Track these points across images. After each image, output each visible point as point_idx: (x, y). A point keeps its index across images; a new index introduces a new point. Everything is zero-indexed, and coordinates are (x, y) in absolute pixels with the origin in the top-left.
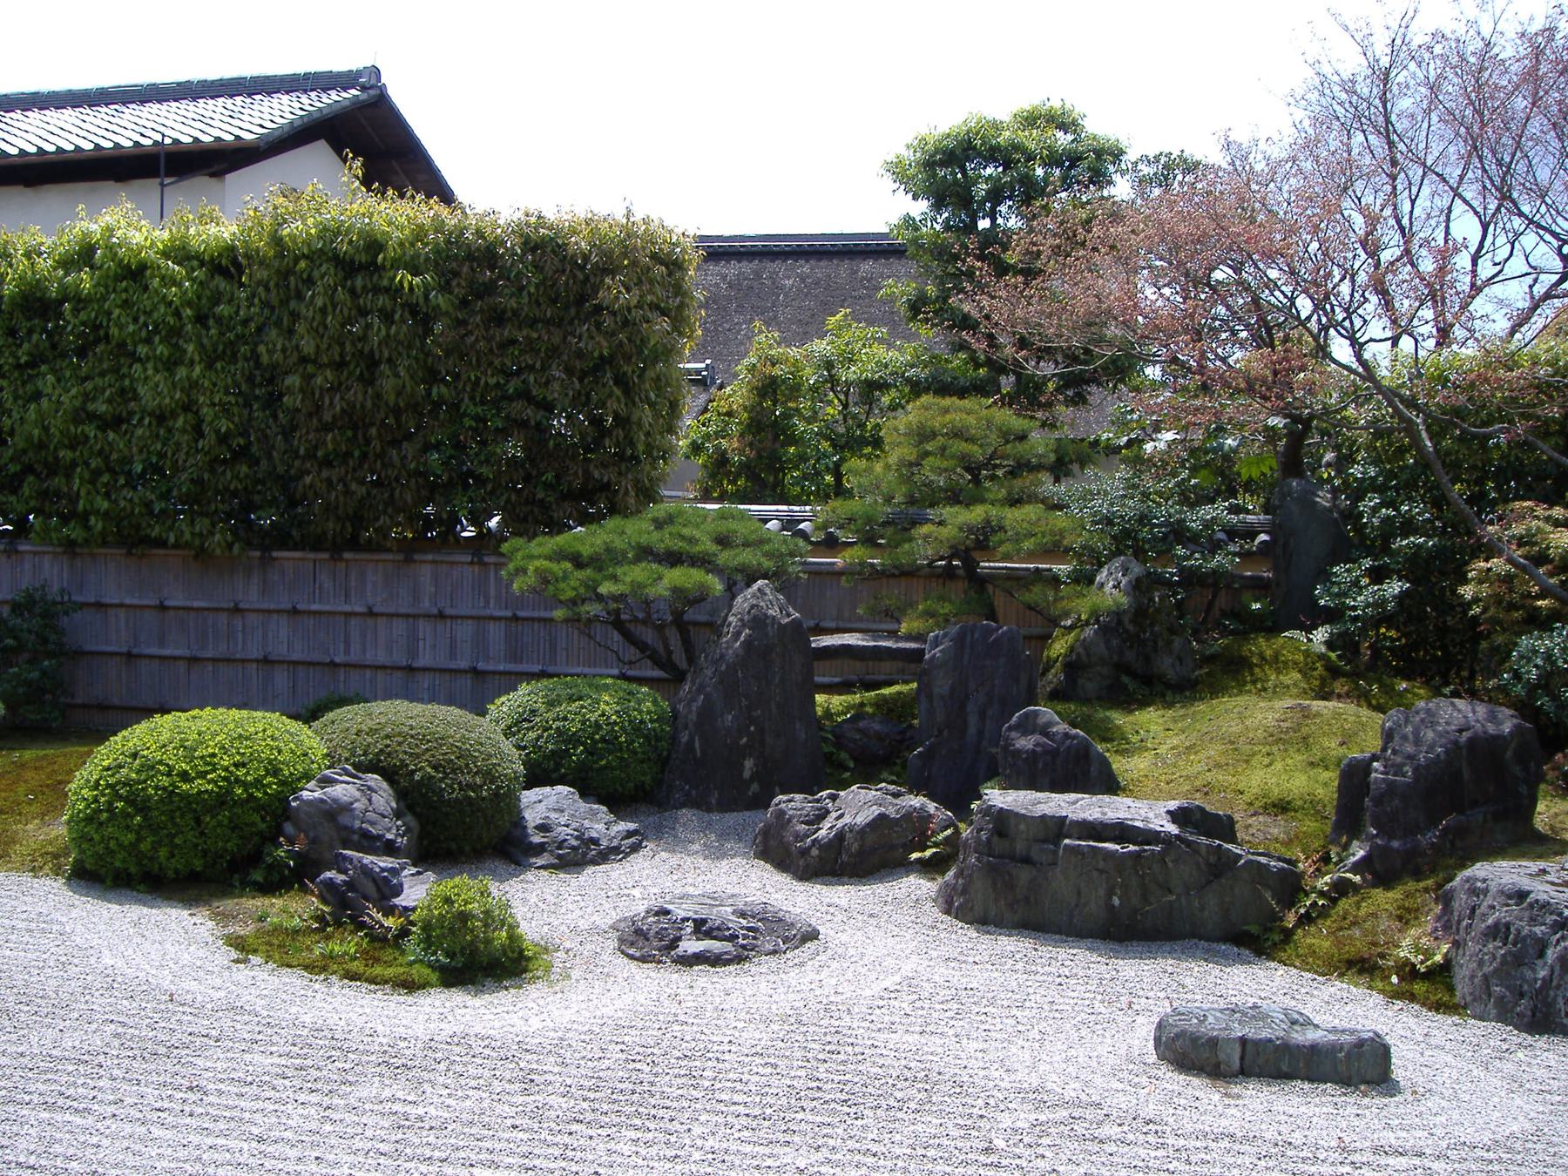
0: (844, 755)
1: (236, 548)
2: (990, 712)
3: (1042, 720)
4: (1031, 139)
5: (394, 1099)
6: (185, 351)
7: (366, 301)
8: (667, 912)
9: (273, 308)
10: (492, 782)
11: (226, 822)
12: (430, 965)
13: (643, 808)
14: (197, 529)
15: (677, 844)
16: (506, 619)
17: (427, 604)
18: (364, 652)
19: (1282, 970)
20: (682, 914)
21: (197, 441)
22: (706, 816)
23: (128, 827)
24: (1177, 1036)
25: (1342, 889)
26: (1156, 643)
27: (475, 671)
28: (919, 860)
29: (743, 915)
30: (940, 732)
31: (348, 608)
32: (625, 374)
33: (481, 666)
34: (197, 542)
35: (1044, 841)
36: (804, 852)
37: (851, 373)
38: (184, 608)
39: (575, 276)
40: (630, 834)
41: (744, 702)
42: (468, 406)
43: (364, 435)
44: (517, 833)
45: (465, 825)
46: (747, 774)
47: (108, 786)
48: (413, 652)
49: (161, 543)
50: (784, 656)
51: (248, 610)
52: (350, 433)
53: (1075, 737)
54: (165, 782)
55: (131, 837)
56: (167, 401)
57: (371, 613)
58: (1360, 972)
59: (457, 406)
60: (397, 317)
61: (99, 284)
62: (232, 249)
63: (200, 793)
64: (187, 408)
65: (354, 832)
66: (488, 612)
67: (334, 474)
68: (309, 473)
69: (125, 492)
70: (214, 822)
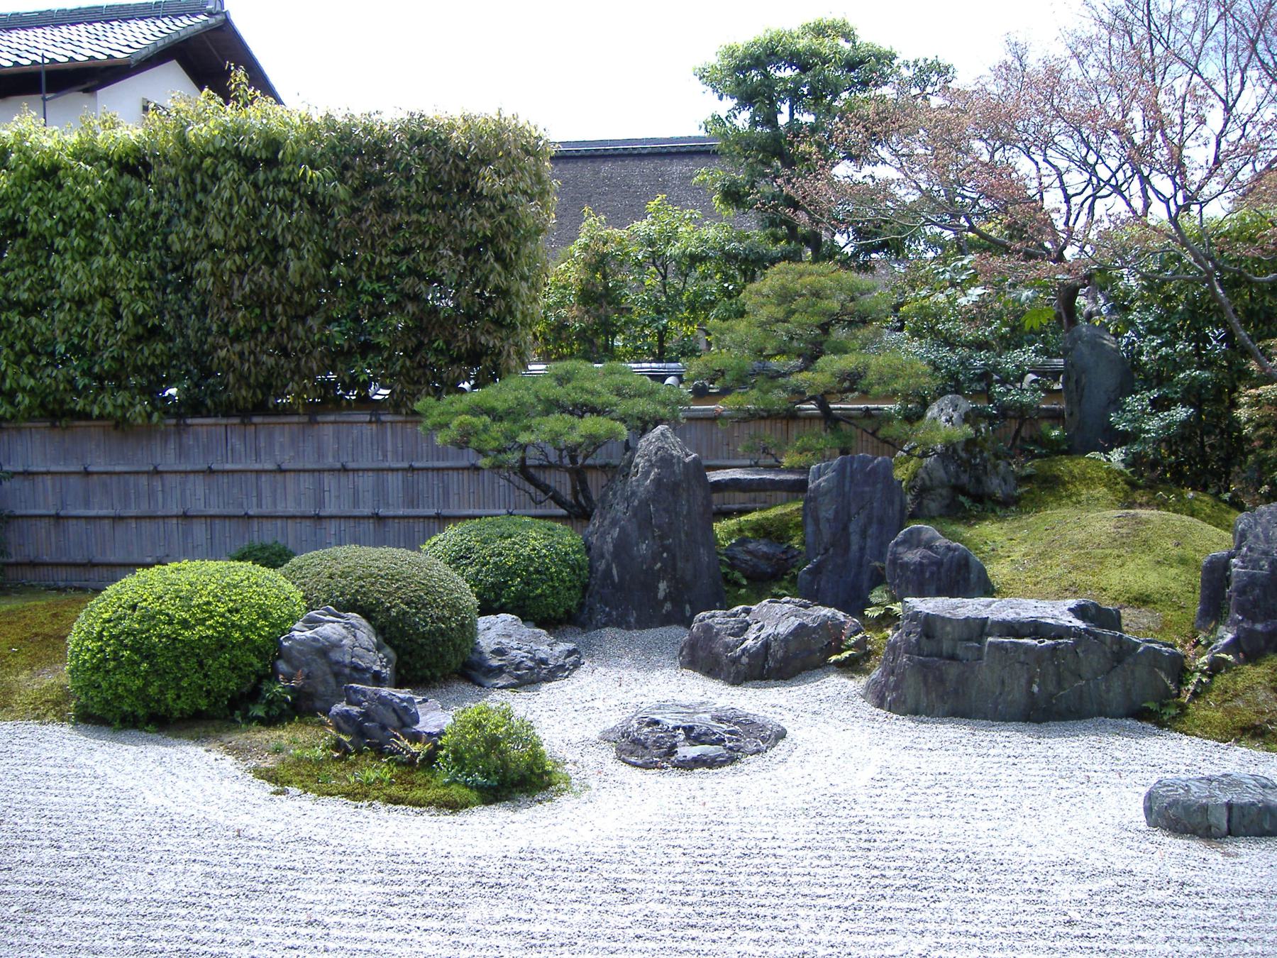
0: (737, 574)
1: (155, 417)
2: (870, 532)
3: (925, 536)
4: (825, 46)
5: (508, 919)
6: (101, 244)
7: (269, 193)
8: (657, 723)
9: (180, 202)
10: (458, 614)
11: (227, 664)
12: (466, 785)
13: (569, 629)
14: (119, 401)
15: (607, 659)
16: (403, 470)
17: (331, 460)
18: (275, 504)
19: (1186, 739)
20: (672, 724)
21: (113, 322)
22: (628, 634)
23: (135, 674)
24: (1170, 805)
25: (1216, 667)
26: (985, 467)
27: (377, 518)
28: (836, 662)
29: (720, 720)
30: (826, 550)
31: (258, 466)
32: (503, 251)
33: (382, 512)
34: (119, 413)
35: (969, 640)
36: (735, 661)
37: (674, 250)
38: (106, 473)
39: (457, 166)
40: (570, 653)
41: (657, 533)
42: (365, 284)
43: (271, 313)
44: (475, 657)
45: (431, 654)
46: (661, 595)
47: (112, 636)
48: (321, 503)
49: (86, 416)
50: (686, 490)
51: (167, 472)
52: (258, 311)
53: (955, 549)
54: (167, 630)
55: (139, 683)
56: (87, 287)
57: (281, 470)
58: (1253, 737)
59: (353, 282)
60: (296, 205)
61: (15, 184)
62: (136, 150)
63: (201, 638)
64: (104, 294)
65: (345, 666)
66: (386, 465)
67: (246, 346)
68: (222, 348)
69: (49, 370)
70: (216, 665)
